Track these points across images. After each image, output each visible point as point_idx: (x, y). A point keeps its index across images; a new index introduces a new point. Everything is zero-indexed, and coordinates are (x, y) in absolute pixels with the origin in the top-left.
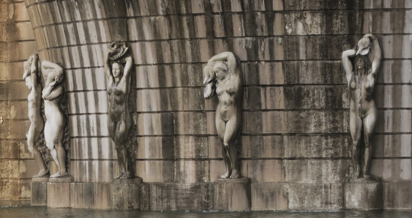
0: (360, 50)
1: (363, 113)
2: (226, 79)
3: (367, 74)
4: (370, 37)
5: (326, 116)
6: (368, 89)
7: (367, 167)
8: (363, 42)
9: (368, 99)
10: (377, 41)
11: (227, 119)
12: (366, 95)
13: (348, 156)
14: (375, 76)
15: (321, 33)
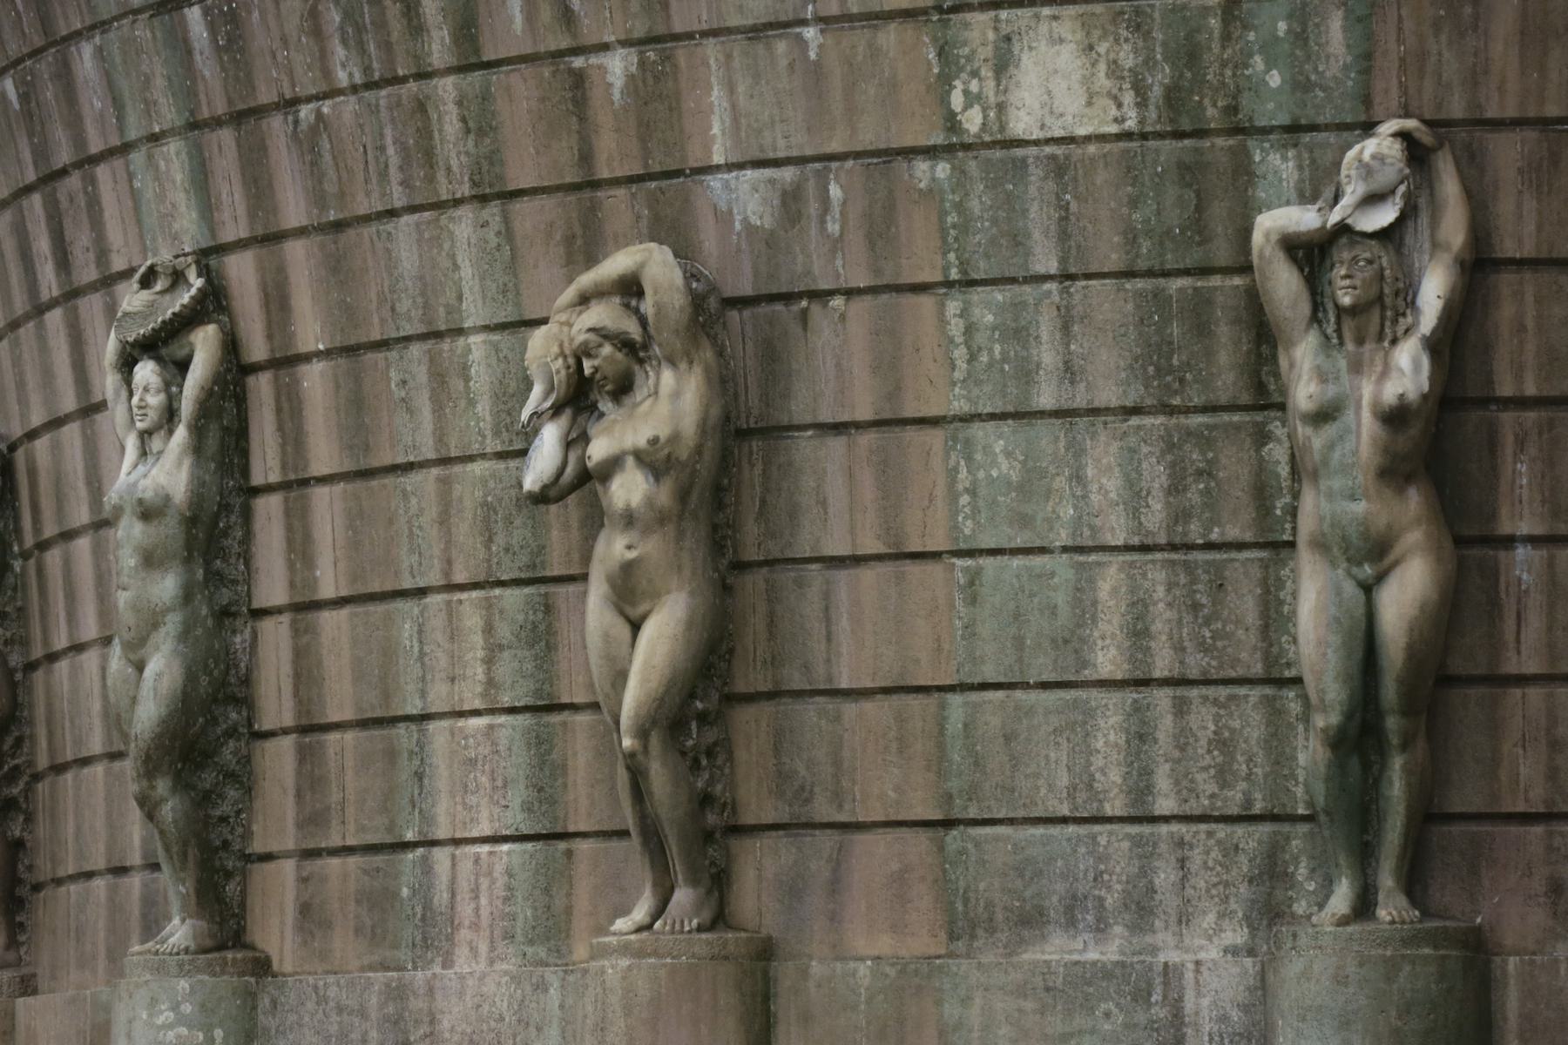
0: (1347, 200)
1: (1373, 554)
2: (640, 393)
3: (1394, 342)
4: (1403, 135)
5: (430, 54)
6: (1395, 417)
7: (1401, 858)
8: (1366, 156)
9: (1394, 472)
10: (1449, 158)
11: (642, 608)
12: (1386, 450)
13: (1181, 709)
14: (1433, 345)
15: (1141, 122)
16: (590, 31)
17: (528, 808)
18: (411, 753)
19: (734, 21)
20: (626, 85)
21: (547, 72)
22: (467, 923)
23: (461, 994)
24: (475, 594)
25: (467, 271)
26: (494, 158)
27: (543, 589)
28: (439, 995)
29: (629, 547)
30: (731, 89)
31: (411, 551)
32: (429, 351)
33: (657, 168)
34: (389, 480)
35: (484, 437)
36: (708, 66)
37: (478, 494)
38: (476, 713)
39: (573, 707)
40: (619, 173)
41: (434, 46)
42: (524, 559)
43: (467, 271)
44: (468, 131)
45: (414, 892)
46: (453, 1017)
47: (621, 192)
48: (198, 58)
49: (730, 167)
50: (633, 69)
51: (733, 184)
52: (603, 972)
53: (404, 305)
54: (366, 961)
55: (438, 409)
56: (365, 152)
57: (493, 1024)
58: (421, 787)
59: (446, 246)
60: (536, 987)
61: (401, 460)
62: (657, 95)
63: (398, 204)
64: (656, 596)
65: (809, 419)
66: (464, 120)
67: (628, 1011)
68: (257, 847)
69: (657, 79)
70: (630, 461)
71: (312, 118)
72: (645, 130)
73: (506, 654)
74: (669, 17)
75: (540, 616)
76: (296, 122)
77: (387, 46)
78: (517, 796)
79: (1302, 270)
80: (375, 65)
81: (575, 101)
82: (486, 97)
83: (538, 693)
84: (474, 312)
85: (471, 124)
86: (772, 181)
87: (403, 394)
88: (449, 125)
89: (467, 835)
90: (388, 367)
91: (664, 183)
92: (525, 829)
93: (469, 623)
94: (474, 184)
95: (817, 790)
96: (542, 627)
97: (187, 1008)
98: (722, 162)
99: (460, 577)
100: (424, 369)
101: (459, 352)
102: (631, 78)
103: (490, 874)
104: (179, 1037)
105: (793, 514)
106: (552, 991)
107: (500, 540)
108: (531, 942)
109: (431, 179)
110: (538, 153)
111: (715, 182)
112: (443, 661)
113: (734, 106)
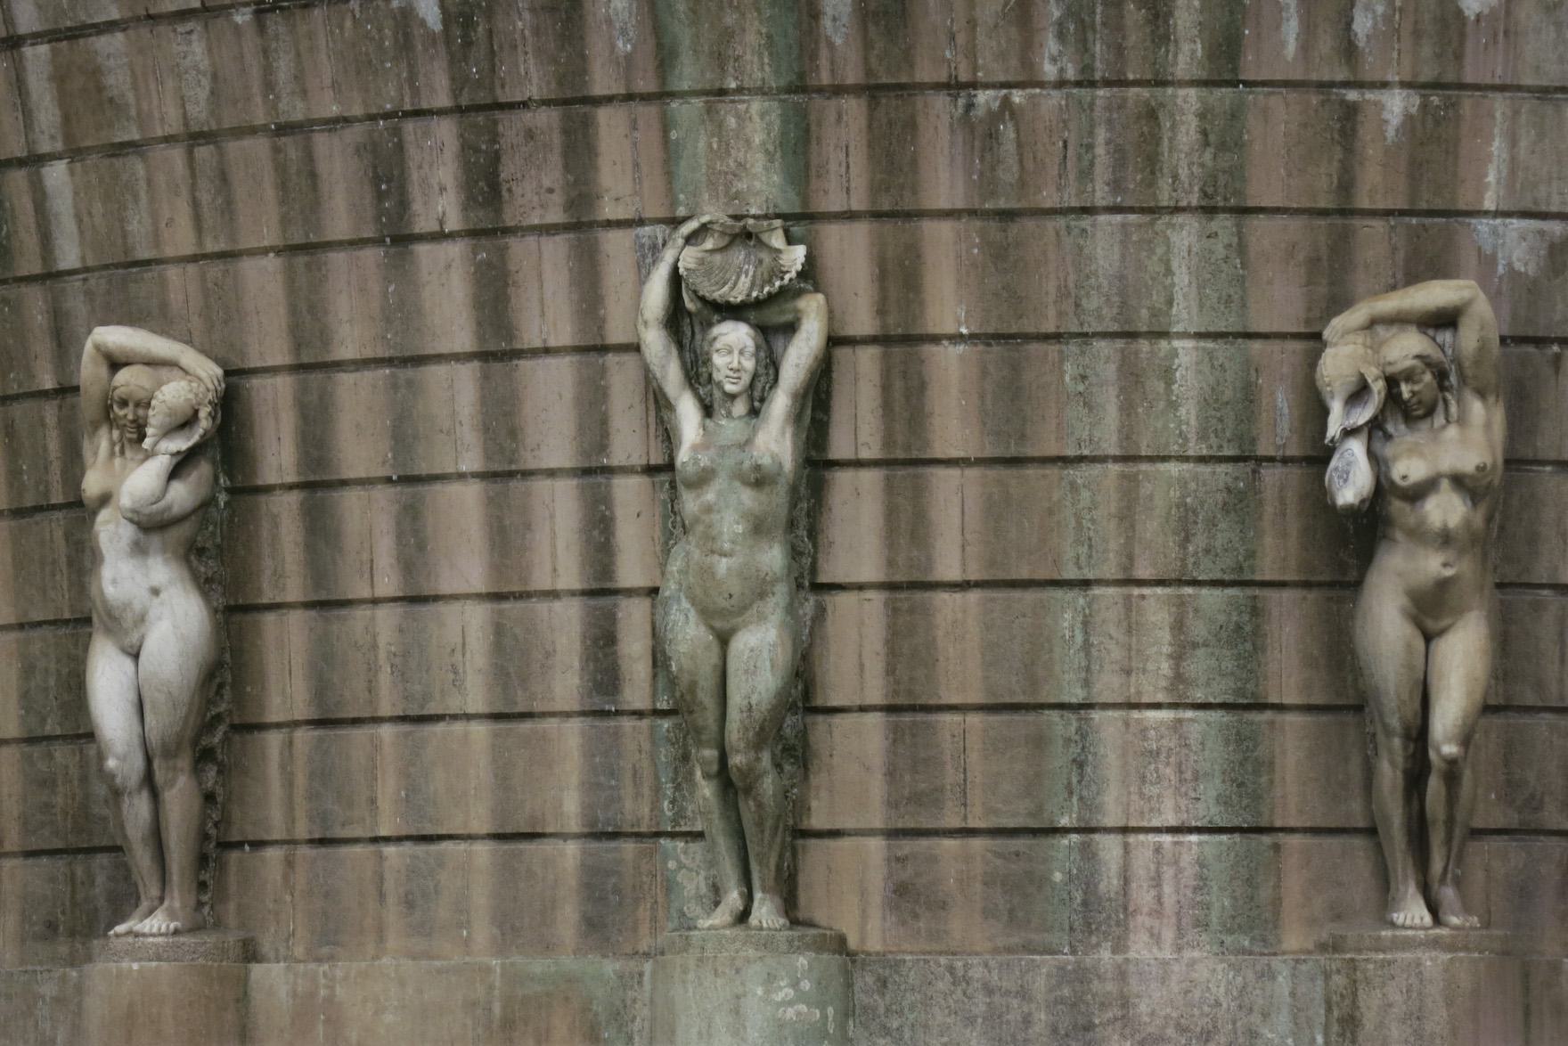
5: (1175, 63)
16: (1370, 70)
17: (1223, 801)
18: (1068, 741)
19: (1528, 81)
20: (1403, 124)
21: (1315, 100)
22: (1145, 910)
23: (1164, 980)
24: (1159, 590)
25: (1182, 278)
26: (1237, 172)
27: (1250, 592)
28: (1133, 981)
29: (1445, 565)
30: (1513, 142)
31: (1078, 542)
32: (1122, 350)
33: (1424, 206)
34: (1052, 472)
35: (1186, 440)
36: (1493, 117)
37: (1174, 494)
38: (1157, 706)
39: (1280, 708)
40: (1381, 206)
41: (1180, 57)
42: (1228, 561)
43: (1182, 278)
44: (1207, 144)
45: (1071, 878)
46: (1152, 1003)
47: (1378, 225)
48: (827, 23)
49: (1498, 214)
50: (1414, 110)
51: (1501, 230)
52: (1419, 965)
53: (1092, 303)
54: (1000, 942)
55: (1127, 409)
56: (1065, 146)
57: (1206, 1009)
58: (1082, 775)
59: (1160, 251)
60: (1261, 976)
61: (1070, 452)
62: (1434, 139)
63: (1100, 203)
64: (1459, 612)
65: (1553, 455)
66: (1205, 133)
67: (1449, 1003)
68: (817, 821)
69: (1437, 123)
70: (1445, 484)
71: (996, 105)
72: (1416, 170)
73: (1201, 652)
74: (1461, 67)
75: (1246, 617)
76: (970, 106)
77: (1119, 50)
78: (1211, 789)
79: (1309, 309)
80: (1098, 64)
81: (1343, 132)
82: (1235, 115)
83: (1239, 692)
84: (1185, 315)
85: (1212, 138)
86: (1541, 233)
87: (1081, 388)
88: (1187, 132)
89: (1145, 824)
90: (1062, 361)
91: (1428, 221)
92: (1220, 822)
93: (1153, 619)
94: (1205, 194)
95: (1547, 799)
96: (1248, 628)
97: (806, 985)
98: (1493, 208)
99: (1142, 572)
100: (1112, 367)
101: (1162, 354)
102: (1408, 118)
103: (1176, 862)
104: (799, 1014)
105: (1533, 539)
106: (1280, 979)
107: (1200, 541)
108: (1230, 931)
109: (1151, 183)
110: (1289, 175)
111: (1483, 226)
112: (1117, 653)
113: (1513, 159)
